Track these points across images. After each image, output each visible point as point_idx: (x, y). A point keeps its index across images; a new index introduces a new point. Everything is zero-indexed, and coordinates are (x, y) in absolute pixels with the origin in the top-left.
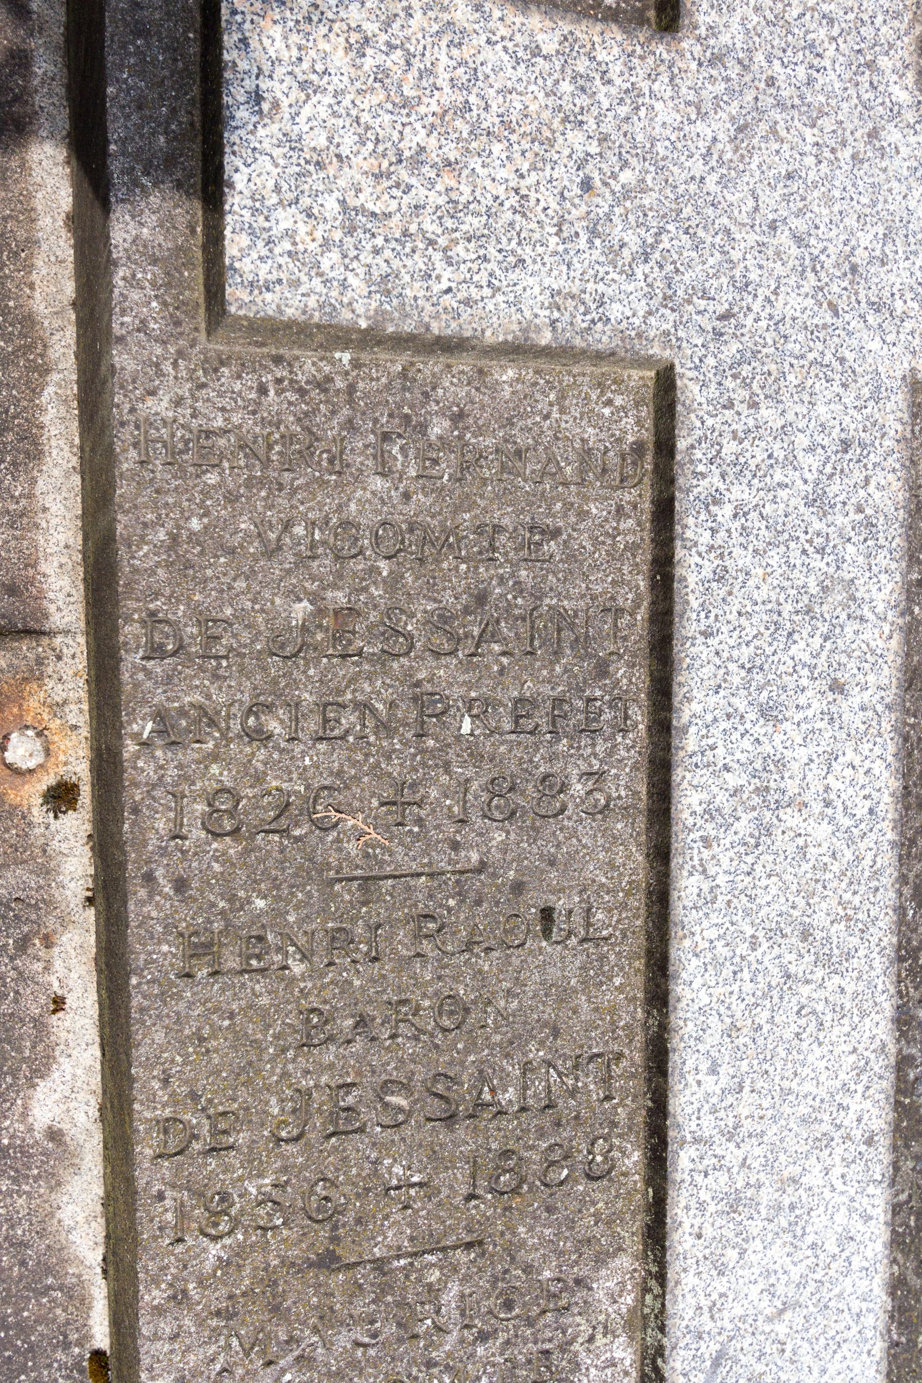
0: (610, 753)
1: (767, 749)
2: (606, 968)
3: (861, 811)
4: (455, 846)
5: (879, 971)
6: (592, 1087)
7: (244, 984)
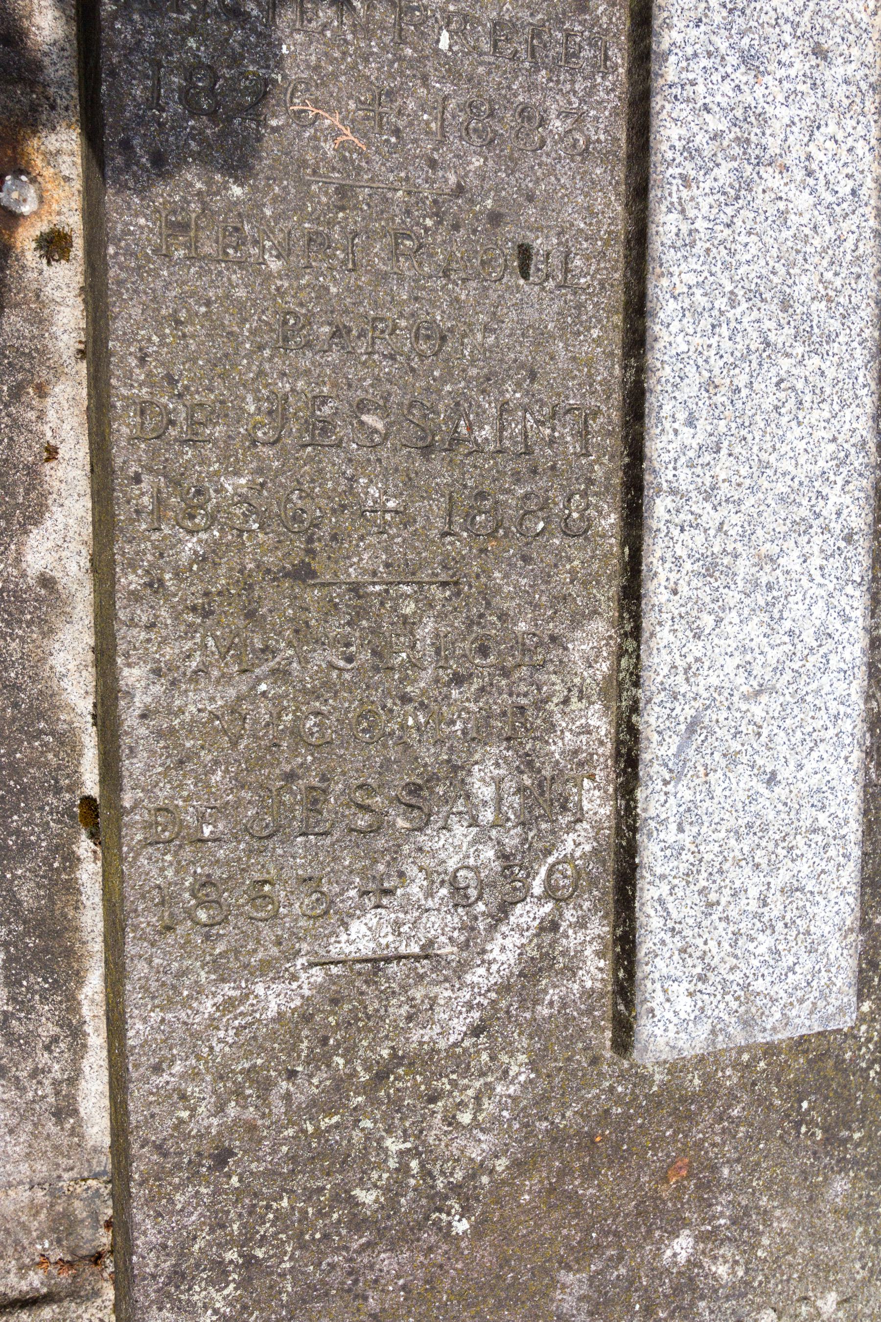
0: (591, 91)
1: (749, 99)
2: (584, 318)
3: (844, 189)
4: (433, 164)
5: (860, 363)
6: (569, 439)
7: (220, 272)
